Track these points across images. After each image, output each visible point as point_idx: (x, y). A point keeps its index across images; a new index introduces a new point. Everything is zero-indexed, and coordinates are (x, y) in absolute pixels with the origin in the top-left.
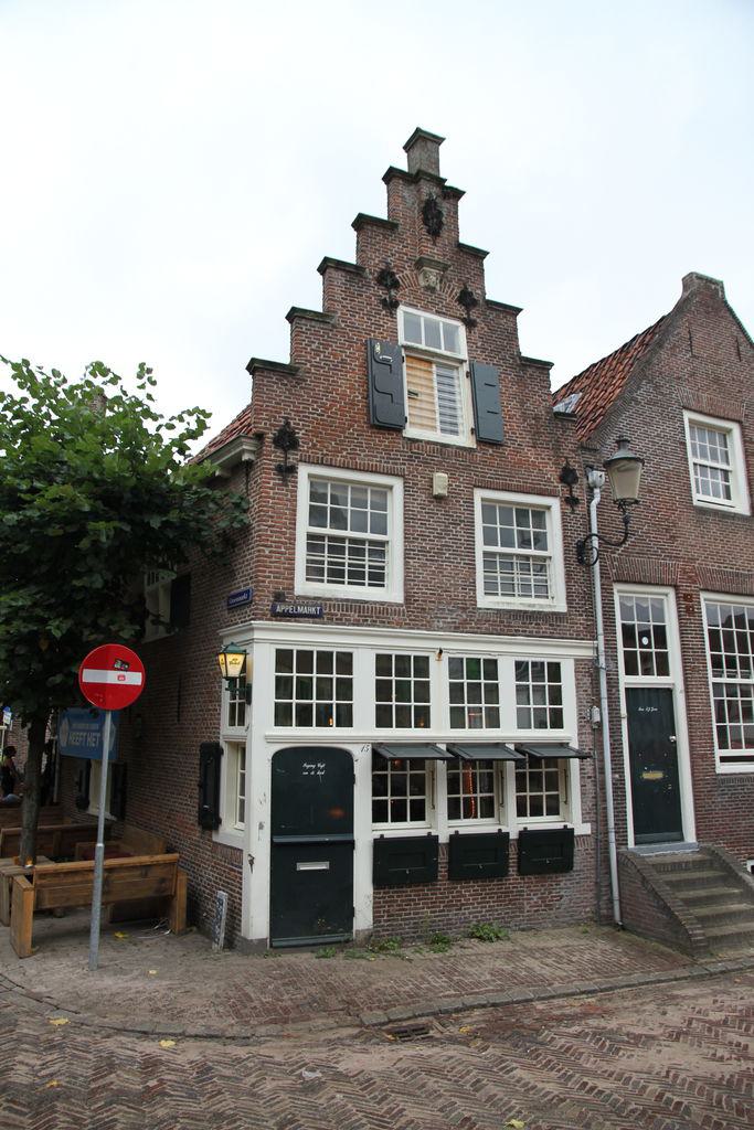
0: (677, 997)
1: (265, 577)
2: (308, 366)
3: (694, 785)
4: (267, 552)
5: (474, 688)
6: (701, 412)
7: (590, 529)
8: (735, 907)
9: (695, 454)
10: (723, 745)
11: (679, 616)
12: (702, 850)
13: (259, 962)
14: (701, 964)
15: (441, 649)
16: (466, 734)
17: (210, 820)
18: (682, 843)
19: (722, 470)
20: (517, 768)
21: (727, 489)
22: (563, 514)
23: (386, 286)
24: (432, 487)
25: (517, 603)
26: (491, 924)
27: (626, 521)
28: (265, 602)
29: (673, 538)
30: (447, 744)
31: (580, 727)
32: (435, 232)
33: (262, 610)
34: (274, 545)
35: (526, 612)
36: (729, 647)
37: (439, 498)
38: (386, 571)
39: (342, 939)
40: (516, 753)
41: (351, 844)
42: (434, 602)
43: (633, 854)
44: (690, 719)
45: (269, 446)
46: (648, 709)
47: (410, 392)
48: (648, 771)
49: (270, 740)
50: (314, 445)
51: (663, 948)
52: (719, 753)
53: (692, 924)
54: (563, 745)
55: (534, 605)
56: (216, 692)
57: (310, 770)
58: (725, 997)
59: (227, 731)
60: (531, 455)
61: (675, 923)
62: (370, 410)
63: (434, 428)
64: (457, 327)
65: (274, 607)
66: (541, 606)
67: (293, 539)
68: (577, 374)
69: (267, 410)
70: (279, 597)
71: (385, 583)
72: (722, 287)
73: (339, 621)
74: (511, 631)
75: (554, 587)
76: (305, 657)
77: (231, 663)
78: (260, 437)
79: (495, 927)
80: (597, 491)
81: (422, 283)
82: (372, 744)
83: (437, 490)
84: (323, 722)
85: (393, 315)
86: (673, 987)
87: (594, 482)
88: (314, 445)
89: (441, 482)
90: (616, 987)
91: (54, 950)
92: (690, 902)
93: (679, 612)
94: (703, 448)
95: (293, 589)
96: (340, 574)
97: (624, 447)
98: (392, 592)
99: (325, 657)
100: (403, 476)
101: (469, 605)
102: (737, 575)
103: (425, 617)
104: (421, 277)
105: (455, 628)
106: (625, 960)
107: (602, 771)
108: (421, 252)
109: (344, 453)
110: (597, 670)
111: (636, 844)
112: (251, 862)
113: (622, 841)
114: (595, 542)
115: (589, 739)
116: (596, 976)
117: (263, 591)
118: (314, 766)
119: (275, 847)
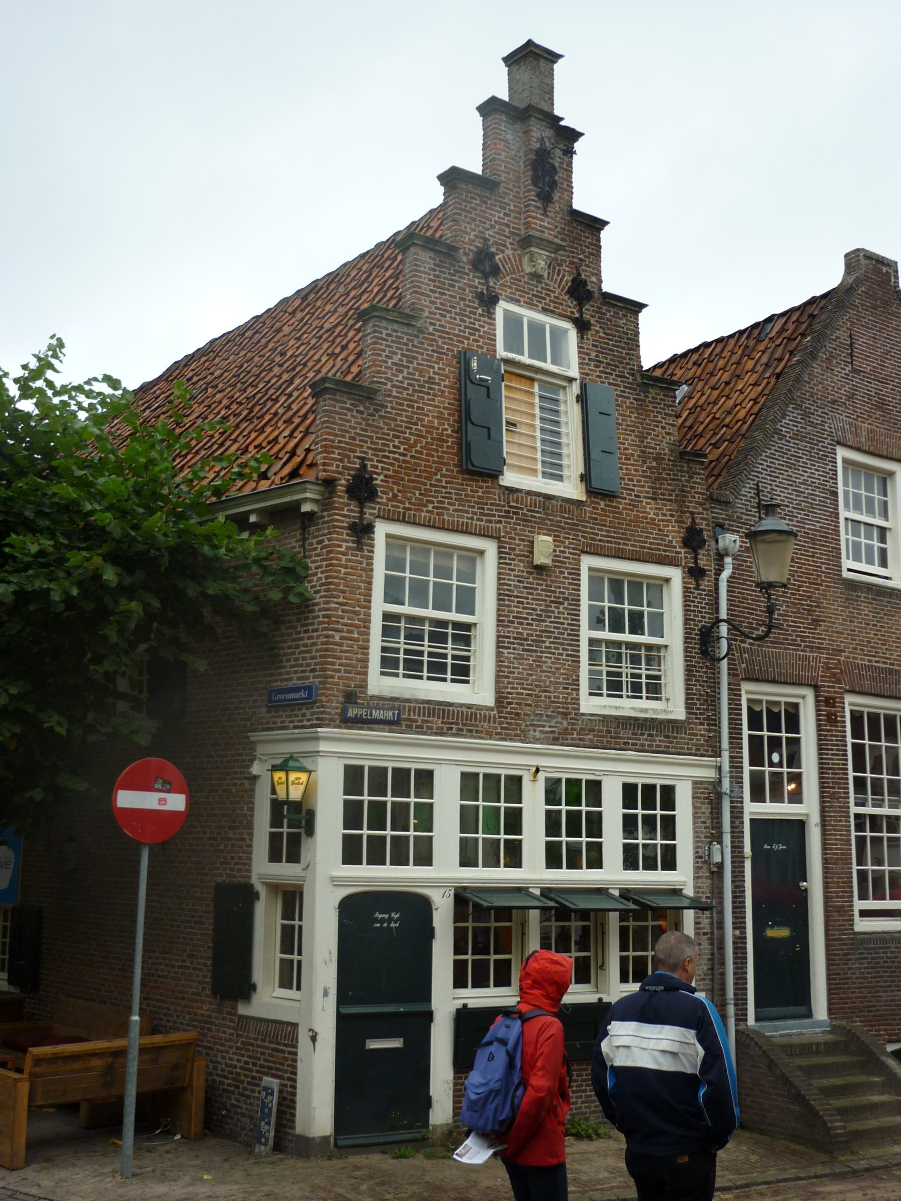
0: (821, 1193)
1: (334, 670)
2: (389, 387)
3: (827, 946)
4: (337, 639)
5: (574, 818)
6: (859, 450)
7: (717, 610)
8: (876, 1098)
9: (847, 505)
10: (863, 896)
11: (819, 726)
12: (834, 1030)
13: (321, 1170)
14: (841, 1162)
15: (538, 764)
16: (564, 876)
17: (235, 982)
18: (807, 1021)
19: (878, 527)
20: (621, 920)
21: (883, 553)
22: (686, 590)
23: (483, 272)
24: (532, 553)
25: (627, 706)
26: (587, 1119)
27: (770, 610)
28: (334, 705)
29: (816, 622)
30: (542, 889)
31: (697, 869)
32: (546, 198)
33: (329, 714)
34: (345, 628)
35: (636, 719)
36: (877, 768)
37: (540, 569)
38: (471, 663)
39: (419, 1136)
40: (542, 899)
41: (428, 1016)
42: (530, 705)
43: (755, 1032)
44: (825, 861)
45: (341, 498)
46: (775, 847)
47: (508, 423)
48: (772, 927)
49: (337, 882)
50: (395, 496)
51: (794, 1146)
52: (859, 905)
53: (830, 1115)
54: (676, 892)
55: (646, 711)
56: (245, 816)
57: (382, 921)
58: (874, 1191)
59: (263, 869)
60: (650, 510)
61: (810, 1115)
62: (464, 449)
63: (534, 472)
64: (566, 331)
65: (344, 711)
66: (655, 711)
67: (367, 621)
68: (680, 352)
69: (339, 448)
70: (350, 698)
71: (471, 678)
72: (897, 271)
73: (420, 730)
74: (619, 743)
75: (669, 686)
76: (378, 774)
77: (293, 783)
78: (329, 483)
79: (592, 1122)
80: (728, 560)
81: (528, 269)
82: (456, 888)
83: (541, 558)
84: (400, 859)
85: (490, 315)
86: (813, 1185)
87: (726, 549)
88: (395, 496)
89: (544, 547)
90: (753, 1185)
91: (47, 1160)
92: (828, 1092)
93: (818, 720)
94: (857, 497)
95: (366, 687)
96: (442, 668)
97: (774, 514)
98: (479, 691)
99: (401, 775)
100: (498, 538)
101: (569, 709)
102: (891, 671)
103: (520, 725)
104: (525, 260)
105: (555, 739)
106: (754, 1158)
107: (721, 926)
108: (528, 226)
109: (430, 507)
110: (719, 795)
111: (757, 1020)
112: (314, 1039)
113: (741, 1017)
114: (724, 629)
115: (706, 884)
116: (726, 1173)
117: (332, 689)
118: (386, 916)
119: (341, 1018)
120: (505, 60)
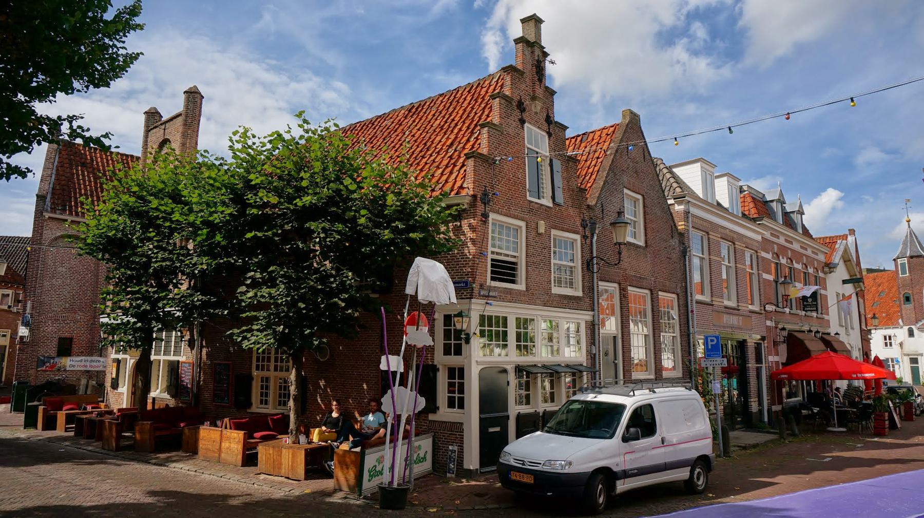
5: (263, 361)
7: (592, 252)
22: (582, 244)
41: (508, 417)
85: (523, 128)
120: (521, 20)
